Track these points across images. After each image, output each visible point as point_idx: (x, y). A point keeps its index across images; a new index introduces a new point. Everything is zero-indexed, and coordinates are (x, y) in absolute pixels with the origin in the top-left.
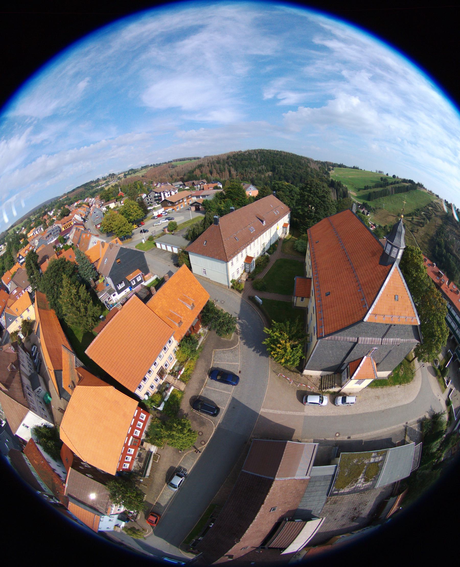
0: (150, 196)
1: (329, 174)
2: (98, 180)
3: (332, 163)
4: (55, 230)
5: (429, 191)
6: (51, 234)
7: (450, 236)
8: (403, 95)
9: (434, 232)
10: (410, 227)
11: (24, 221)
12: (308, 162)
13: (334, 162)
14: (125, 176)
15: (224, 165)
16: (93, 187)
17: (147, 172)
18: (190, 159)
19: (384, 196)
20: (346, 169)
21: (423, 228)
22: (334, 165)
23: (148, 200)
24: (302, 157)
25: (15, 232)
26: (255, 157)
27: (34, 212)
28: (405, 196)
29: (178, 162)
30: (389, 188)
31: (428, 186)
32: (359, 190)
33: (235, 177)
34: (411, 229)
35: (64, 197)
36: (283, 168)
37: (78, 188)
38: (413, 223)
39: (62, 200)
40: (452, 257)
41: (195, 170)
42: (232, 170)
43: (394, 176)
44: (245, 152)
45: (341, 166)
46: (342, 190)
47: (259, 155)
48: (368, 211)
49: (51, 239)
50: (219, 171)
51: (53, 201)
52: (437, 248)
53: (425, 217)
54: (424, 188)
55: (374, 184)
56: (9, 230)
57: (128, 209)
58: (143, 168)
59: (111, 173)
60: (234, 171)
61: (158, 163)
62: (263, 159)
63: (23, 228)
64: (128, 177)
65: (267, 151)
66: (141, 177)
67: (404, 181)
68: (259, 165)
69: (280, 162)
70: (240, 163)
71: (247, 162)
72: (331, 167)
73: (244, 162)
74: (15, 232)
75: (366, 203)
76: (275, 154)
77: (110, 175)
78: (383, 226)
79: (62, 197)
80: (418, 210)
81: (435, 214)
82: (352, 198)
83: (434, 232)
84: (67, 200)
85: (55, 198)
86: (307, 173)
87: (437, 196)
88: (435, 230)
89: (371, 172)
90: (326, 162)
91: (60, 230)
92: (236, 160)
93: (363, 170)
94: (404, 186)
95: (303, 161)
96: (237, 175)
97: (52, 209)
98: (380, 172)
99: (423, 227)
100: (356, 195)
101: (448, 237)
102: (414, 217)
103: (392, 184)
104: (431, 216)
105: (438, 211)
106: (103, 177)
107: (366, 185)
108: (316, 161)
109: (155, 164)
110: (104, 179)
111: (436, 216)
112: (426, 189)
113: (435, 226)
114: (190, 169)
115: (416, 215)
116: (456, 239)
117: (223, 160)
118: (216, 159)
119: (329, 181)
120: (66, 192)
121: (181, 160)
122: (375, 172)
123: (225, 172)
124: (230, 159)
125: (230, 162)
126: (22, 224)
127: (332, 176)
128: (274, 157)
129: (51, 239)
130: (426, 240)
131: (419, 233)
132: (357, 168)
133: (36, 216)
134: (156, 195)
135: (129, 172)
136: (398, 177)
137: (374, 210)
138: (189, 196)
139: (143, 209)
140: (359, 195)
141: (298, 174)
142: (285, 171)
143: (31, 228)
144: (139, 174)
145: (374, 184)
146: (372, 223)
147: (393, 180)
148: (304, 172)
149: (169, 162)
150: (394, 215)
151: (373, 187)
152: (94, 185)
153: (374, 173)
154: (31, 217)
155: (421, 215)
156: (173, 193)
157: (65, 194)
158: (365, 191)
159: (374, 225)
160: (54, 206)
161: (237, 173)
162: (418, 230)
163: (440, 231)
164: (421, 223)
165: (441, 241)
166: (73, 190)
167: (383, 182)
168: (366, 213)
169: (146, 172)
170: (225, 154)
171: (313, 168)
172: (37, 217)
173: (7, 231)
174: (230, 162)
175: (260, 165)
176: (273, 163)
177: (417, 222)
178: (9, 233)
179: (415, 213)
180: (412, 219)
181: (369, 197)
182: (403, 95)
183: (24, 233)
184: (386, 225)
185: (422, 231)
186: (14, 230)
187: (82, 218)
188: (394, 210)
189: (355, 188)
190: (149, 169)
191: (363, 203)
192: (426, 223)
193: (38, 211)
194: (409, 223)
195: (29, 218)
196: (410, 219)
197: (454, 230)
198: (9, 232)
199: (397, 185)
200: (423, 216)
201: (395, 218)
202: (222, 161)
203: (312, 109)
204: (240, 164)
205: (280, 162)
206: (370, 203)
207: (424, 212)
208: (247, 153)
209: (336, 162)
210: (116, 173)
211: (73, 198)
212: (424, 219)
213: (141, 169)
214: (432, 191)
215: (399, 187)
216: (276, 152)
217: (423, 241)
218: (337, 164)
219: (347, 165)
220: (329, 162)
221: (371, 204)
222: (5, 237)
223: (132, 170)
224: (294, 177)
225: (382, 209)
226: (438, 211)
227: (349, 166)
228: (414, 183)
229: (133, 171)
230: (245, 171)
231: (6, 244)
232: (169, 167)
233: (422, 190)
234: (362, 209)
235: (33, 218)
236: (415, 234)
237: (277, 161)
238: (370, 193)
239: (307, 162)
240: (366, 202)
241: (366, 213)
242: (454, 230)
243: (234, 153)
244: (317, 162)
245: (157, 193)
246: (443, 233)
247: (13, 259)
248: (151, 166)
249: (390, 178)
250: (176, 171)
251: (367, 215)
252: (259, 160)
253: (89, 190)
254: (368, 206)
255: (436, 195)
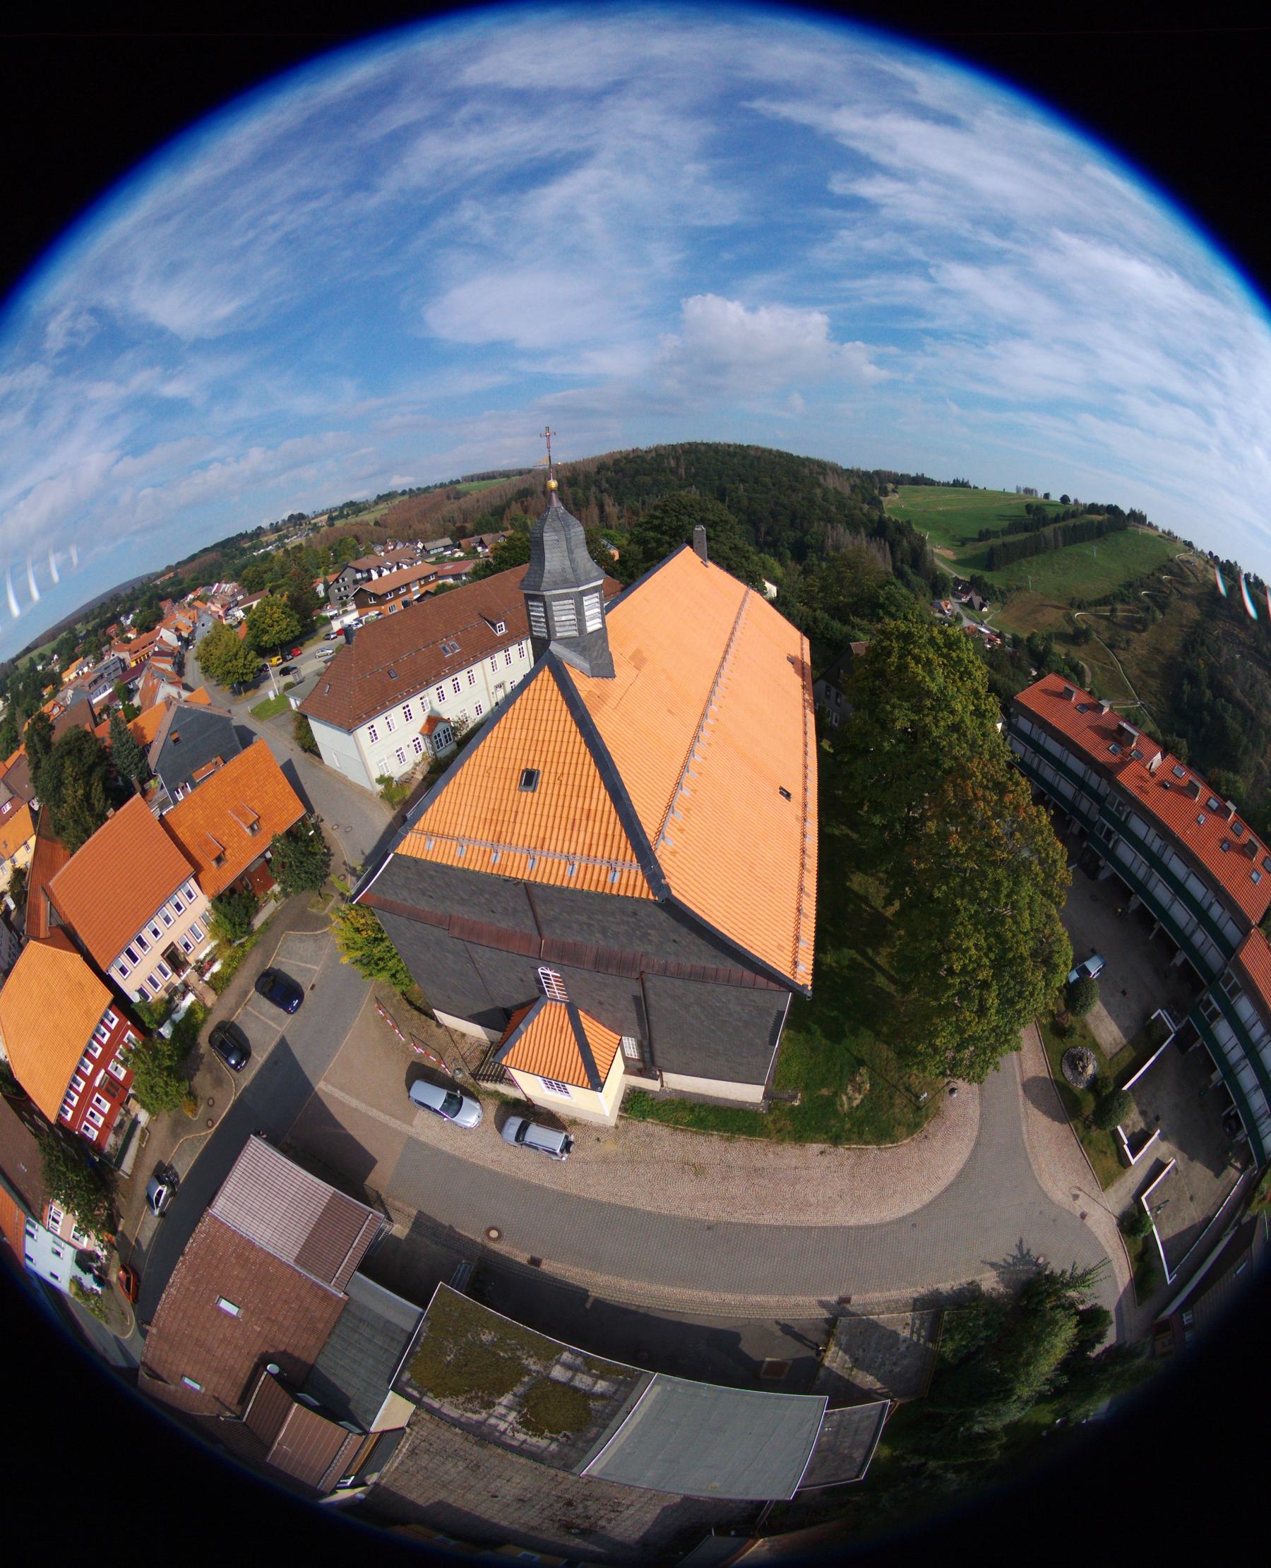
0: (343, 580)
1: (880, 502)
2: (259, 532)
3: (896, 475)
4: (112, 668)
5: (1164, 532)
6: (102, 676)
7: (1225, 650)
8: (1053, 289)
9: (1177, 645)
10: (1106, 635)
11: (60, 637)
12: (820, 473)
13: (900, 470)
14: (331, 520)
15: (587, 488)
16: (243, 552)
17: (390, 509)
18: (506, 475)
19: (1031, 555)
20: (931, 487)
21: (1144, 634)
22: (900, 480)
23: (339, 590)
24: (808, 459)
25: (33, 665)
26: (673, 463)
27: (84, 615)
28: (1093, 550)
29: (475, 483)
30: (1048, 531)
31: (1162, 517)
32: (963, 542)
33: (614, 522)
34: (1108, 641)
35: (167, 577)
36: (745, 490)
37: (206, 550)
38: (1114, 624)
39: (162, 583)
40: (1230, 707)
41: (508, 505)
42: (608, 500)
43: (1065, 499)
44: (649, 452)
45: (919, 481)
46: (909, 543)
47: (682, 458)
48: (985, 600)
49: (101, 689)
50: (572, 507)
51: (137, 587)
52: (1185, 687)
53: (1151, 604)
54: (1150, 525)
55: (1006, 524)
56: (19, 657)
57: (260, 617)
58: (381, 499)
59: (295, 513)
60: (614, 505)
61: (423, 486)
62: (693, 470)
63: (56, 657)
64: (339, 524)
65: (708, 446)
66: (372, 524)
67: (1094, 508)
68: (681, 487)
69: (739, 476)
70: (631, 483)
71: (648, 479)
72: (890, 486)
73: (640, 479)
74: (33, 665)
75: (981, 578)
76: (729, 454)
77: (291, 517)
78: (1024, 635)
79: (162, 574)
80: (1130, 585)
81: (1180, 593)
82: (938, 562)
83: (1177, 645)
84: (172, 584)
85: (144, 577)
86: (811, 502)
87: (1189, 545)
88: (1180, 638)
89: (1004, 493)
90: (877, 473)
91: (124, 668)
92: (621, 474)
93: (981, 487)
94: (1092, 523)
95: (806, 471)
96: (622, 517)
97: (131, 610)
98: (1028, 491)
99: (1144, 631)
100: (954, 558)
101: (1218, 655)
102: (1119, 606)
103: (1057, 519)
104: (1166, 598)
105: (1188, 585)
106: (272, 524)
107: (984, 527)
108: (848, 470)
109: (414, 488)
110: (275, 528)
111: (1184, 597)
112: (1156, 528)
113: (1181, 626)
114: (497, 502)
115: (1123, 601)
116: (1243, 656)
117: (587, 475)
118: (568, 474)
119: (872, 521)
120: (173, 563)
121: (482, 477)
122: (1014, 491)
123: (587, 507)
124: (604, 472)
125: (604, 482)
126: (54, 644)
127: (890, 510)
128: (724, 463)
129: (101, 689)
130: (1154, 667)
131: (1131, 648)
132: (964, 485)
133: (90, 627)
134: (359, 576)
135: (342, 509)
136: (1076, 501)
137: (1002, 593)
138: (399, 589)
139: (297, 616)
140: (962, 556)
141: (784, 507)
142: (750, 500)
143: (73, 659)
144: (368, 517)
145: (1007, 523)
146: (992, 632)
147: (1062, 510)
148: (803, 499)
149: (452, 482)
150: (1060, 605)
151: (1003, 532)
152: (246, 545)
153: (1011, 494)
154: (79, 626)
155: (1138, 599)
156: (386, 573)
157: (169, 569)
158: (981, 543)
159: (999, 635)
160: (137, 598)
161: (621, 511)
162: (1128, 641)
163: (1194, 640)
164: (1139, 620)
165: (1198, 666)
166: (193, 558)
167: (1031, 516)
168: (977, 606)
169: (386, 511)
170: (592, 460)
171: (831, 486)
172: (93, 628)
173: (14, 661)
174: (604, 482)
175: (686, 487)
176: (720, 479)
177: (1126, 618)
178: (20, 666)
179: (1121, 593)
180: (1113, 611)
181: (989, 561)
182: (1053, 289)
183: (57, 669)
184: (1034, 634)
185: (1140, 643)
186: (31, 658)
187: (180, 638)
188: (1059, 590)
189: (953, 538)
190: (396, 501)
191: (972, 577)
192: (1154, 619)
193: (96, 612)
194: (1105, 623)
195: (72, 630)
196: (1105, 611)
197: (1237, 631)
198: (18, 663)
199: (1071, 522)
200: (1144, 602)
201: (1061, 612)
202: (581, 477)
203: (874, 348)
204: (629, 485)
205: (739, 476)
206: (988, 577)
207: (1148, 590)
208: (653, 454)
209: (905, 472)
210: (307, 512)
211: (188, 579)
212: (1147, 609)
213: (376, 503)
214: (1172, 530)
215: (1074, 526)
216: (732, 449)
217: (1144, 672)
218: (908, 476)
219: (936, 479)
220: (885, 472)
221: (993, 579)
222: (8, 677)
223: (351, 504)
224: (773, 515)
225: (1027, 590)
226: (1188, 585)
227: (943, 479)
228: (1122, 513)
229: (355, 507)
230: (644, 503)
231: (8, 695)
232: (448, 498)
233: (1142, 530)
234: (967, 593)
235: (81, 629)
236: (1123, 655)
237: (731, 473)
238: (992, 549)
239: (817, 473)
240: (978, 573)
241: (977, 606)
242: (1237, 631)
243: (618, 456)
244: (850, 472)
245: (361, 571)
246: (1203, 644)
247: (17, 736)
248: (404, 493)
249: (1054, 505)
250: (460, 509)
251: (981, 609)
252: (682, 471)
253: (234, 557)
254: (986, 584)
255: (1185, 542)
